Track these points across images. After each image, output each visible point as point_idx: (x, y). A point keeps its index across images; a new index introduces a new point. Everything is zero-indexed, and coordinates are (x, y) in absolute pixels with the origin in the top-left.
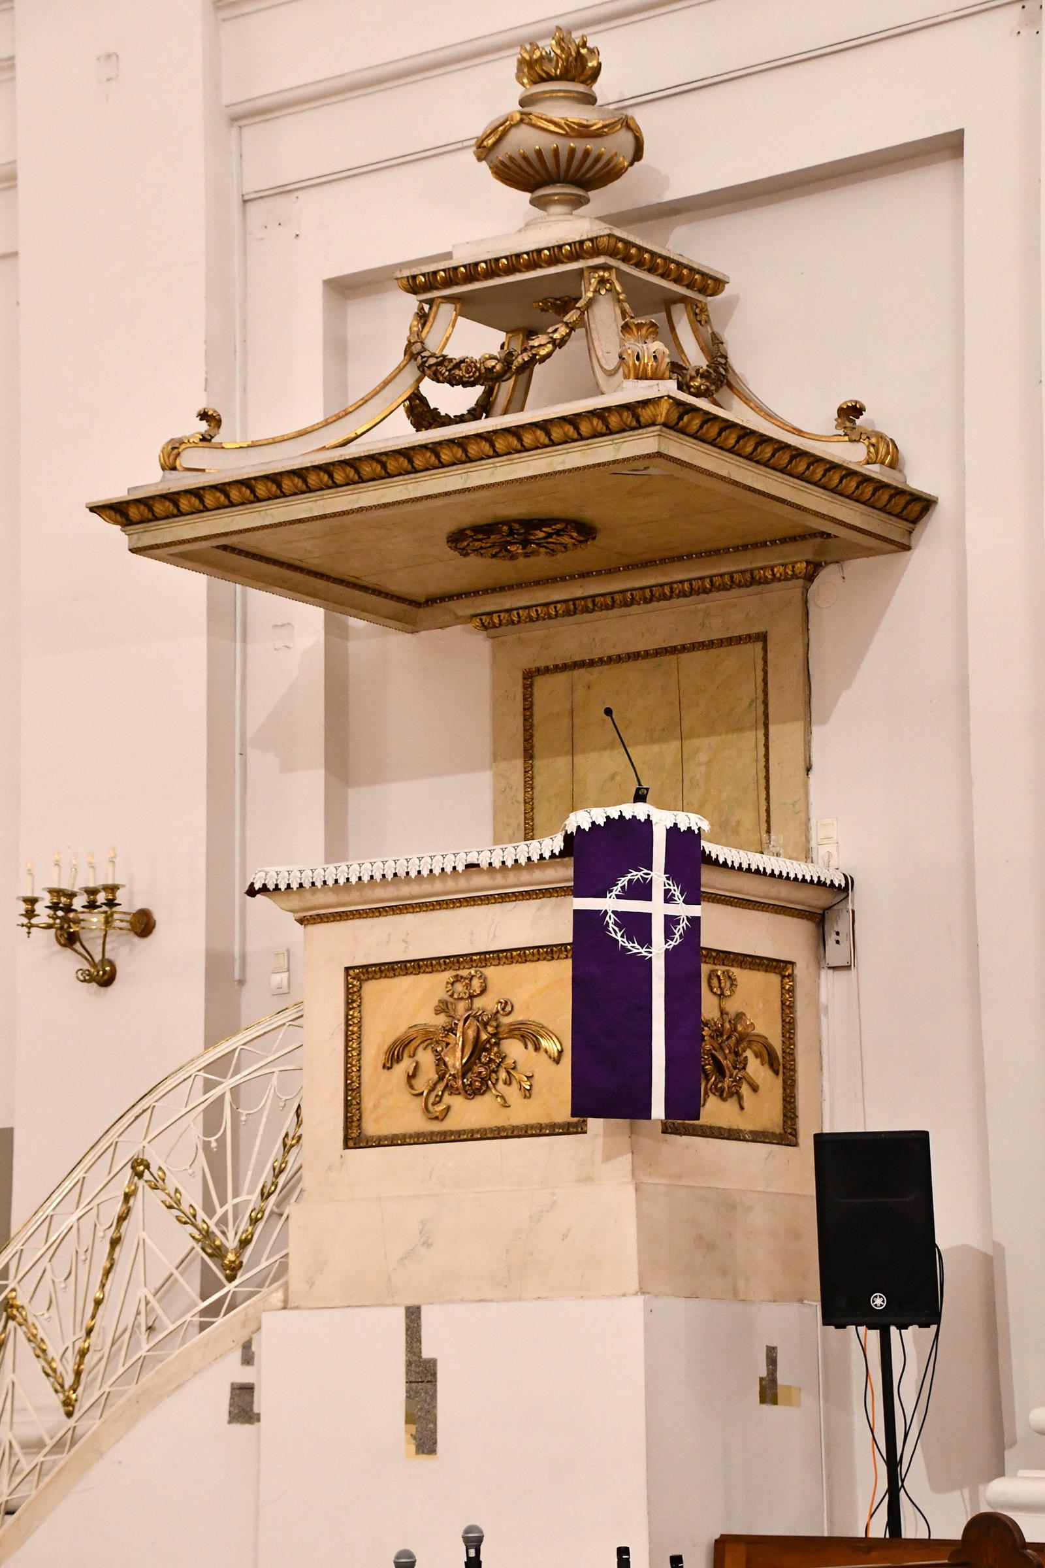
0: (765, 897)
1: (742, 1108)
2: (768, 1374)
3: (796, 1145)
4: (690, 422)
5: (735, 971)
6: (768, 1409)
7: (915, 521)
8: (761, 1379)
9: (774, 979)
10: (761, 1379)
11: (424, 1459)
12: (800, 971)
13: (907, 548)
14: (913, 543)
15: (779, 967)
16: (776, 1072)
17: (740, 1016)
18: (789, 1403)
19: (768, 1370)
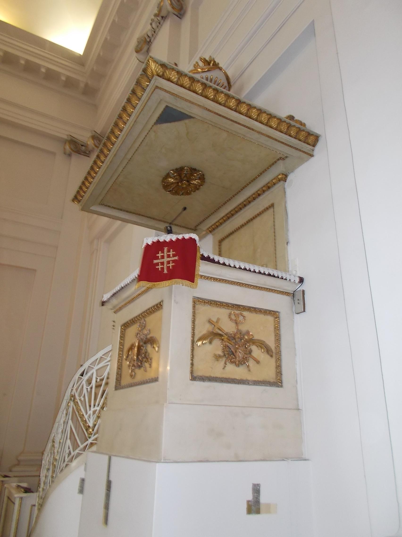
0: (235, 279)
1: (249, 370)
2: (253, 498)
3: (282, 386)
4: (150, 78)
5: (245, 313)
6: (254, 517)
7: (314, 146)
8: (248, 502)
9: (270, 319)
10: (248, 502)
11: (256, 482)
12: (283, 316)
13: (312, 156)
14: (315, 153)
15: (275, 314)
16: (272, 356)
17: (248, 333)
18: (268, 511)
19: (254, 496)
